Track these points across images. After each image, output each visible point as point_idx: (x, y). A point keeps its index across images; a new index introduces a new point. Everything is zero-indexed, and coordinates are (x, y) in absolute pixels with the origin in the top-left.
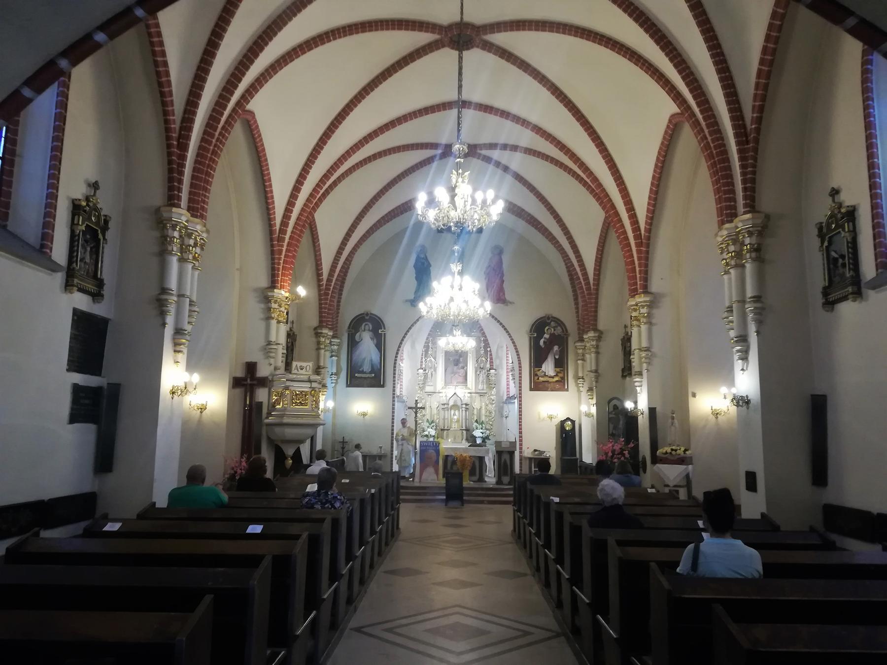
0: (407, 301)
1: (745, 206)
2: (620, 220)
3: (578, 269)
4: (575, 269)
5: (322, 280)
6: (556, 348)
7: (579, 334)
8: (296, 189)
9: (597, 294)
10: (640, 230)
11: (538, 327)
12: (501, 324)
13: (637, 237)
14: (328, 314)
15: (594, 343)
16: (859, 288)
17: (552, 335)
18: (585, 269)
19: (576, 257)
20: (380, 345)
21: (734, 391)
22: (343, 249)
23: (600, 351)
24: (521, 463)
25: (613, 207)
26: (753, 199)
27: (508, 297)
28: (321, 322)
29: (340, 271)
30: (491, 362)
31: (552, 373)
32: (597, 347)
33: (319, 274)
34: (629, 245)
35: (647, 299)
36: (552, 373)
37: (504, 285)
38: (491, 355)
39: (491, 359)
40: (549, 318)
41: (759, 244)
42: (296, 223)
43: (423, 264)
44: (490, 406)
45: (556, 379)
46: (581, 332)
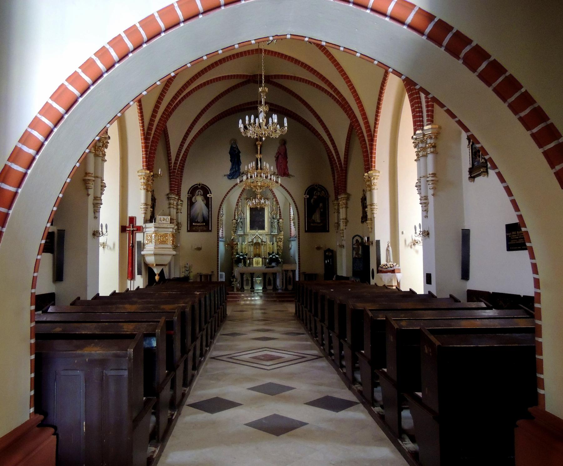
1: (428, 121)
2: (359, 125)
4: (332, 154)
5: (171, 163)
6: (321, 205)
7: (335, 195)
8: (182, 145)
11: (311, 191)
13: (341, 167)
14: (176, 185)
15: (344, 201)
16: (487, 170)
18: (338, 154)
19: (333, 147)
20: (208, 202)
22: (184, 143)
24: (299, 276)
25: (355, 116)
26: (432, 117)
27: (290, 172)
28: (171, 190)
30: (280, 215)
31: (319, 221)
32: (347, 204)
33: (169, 160)
34: (364, 140)
36: (319, 221)
37: (288, 165)
38: (280, 210)
39: (280, 212)
40: (316, 185)
41: (435, 144)
42: (156, 128)
43: (235, 151)
46: (337, 194)
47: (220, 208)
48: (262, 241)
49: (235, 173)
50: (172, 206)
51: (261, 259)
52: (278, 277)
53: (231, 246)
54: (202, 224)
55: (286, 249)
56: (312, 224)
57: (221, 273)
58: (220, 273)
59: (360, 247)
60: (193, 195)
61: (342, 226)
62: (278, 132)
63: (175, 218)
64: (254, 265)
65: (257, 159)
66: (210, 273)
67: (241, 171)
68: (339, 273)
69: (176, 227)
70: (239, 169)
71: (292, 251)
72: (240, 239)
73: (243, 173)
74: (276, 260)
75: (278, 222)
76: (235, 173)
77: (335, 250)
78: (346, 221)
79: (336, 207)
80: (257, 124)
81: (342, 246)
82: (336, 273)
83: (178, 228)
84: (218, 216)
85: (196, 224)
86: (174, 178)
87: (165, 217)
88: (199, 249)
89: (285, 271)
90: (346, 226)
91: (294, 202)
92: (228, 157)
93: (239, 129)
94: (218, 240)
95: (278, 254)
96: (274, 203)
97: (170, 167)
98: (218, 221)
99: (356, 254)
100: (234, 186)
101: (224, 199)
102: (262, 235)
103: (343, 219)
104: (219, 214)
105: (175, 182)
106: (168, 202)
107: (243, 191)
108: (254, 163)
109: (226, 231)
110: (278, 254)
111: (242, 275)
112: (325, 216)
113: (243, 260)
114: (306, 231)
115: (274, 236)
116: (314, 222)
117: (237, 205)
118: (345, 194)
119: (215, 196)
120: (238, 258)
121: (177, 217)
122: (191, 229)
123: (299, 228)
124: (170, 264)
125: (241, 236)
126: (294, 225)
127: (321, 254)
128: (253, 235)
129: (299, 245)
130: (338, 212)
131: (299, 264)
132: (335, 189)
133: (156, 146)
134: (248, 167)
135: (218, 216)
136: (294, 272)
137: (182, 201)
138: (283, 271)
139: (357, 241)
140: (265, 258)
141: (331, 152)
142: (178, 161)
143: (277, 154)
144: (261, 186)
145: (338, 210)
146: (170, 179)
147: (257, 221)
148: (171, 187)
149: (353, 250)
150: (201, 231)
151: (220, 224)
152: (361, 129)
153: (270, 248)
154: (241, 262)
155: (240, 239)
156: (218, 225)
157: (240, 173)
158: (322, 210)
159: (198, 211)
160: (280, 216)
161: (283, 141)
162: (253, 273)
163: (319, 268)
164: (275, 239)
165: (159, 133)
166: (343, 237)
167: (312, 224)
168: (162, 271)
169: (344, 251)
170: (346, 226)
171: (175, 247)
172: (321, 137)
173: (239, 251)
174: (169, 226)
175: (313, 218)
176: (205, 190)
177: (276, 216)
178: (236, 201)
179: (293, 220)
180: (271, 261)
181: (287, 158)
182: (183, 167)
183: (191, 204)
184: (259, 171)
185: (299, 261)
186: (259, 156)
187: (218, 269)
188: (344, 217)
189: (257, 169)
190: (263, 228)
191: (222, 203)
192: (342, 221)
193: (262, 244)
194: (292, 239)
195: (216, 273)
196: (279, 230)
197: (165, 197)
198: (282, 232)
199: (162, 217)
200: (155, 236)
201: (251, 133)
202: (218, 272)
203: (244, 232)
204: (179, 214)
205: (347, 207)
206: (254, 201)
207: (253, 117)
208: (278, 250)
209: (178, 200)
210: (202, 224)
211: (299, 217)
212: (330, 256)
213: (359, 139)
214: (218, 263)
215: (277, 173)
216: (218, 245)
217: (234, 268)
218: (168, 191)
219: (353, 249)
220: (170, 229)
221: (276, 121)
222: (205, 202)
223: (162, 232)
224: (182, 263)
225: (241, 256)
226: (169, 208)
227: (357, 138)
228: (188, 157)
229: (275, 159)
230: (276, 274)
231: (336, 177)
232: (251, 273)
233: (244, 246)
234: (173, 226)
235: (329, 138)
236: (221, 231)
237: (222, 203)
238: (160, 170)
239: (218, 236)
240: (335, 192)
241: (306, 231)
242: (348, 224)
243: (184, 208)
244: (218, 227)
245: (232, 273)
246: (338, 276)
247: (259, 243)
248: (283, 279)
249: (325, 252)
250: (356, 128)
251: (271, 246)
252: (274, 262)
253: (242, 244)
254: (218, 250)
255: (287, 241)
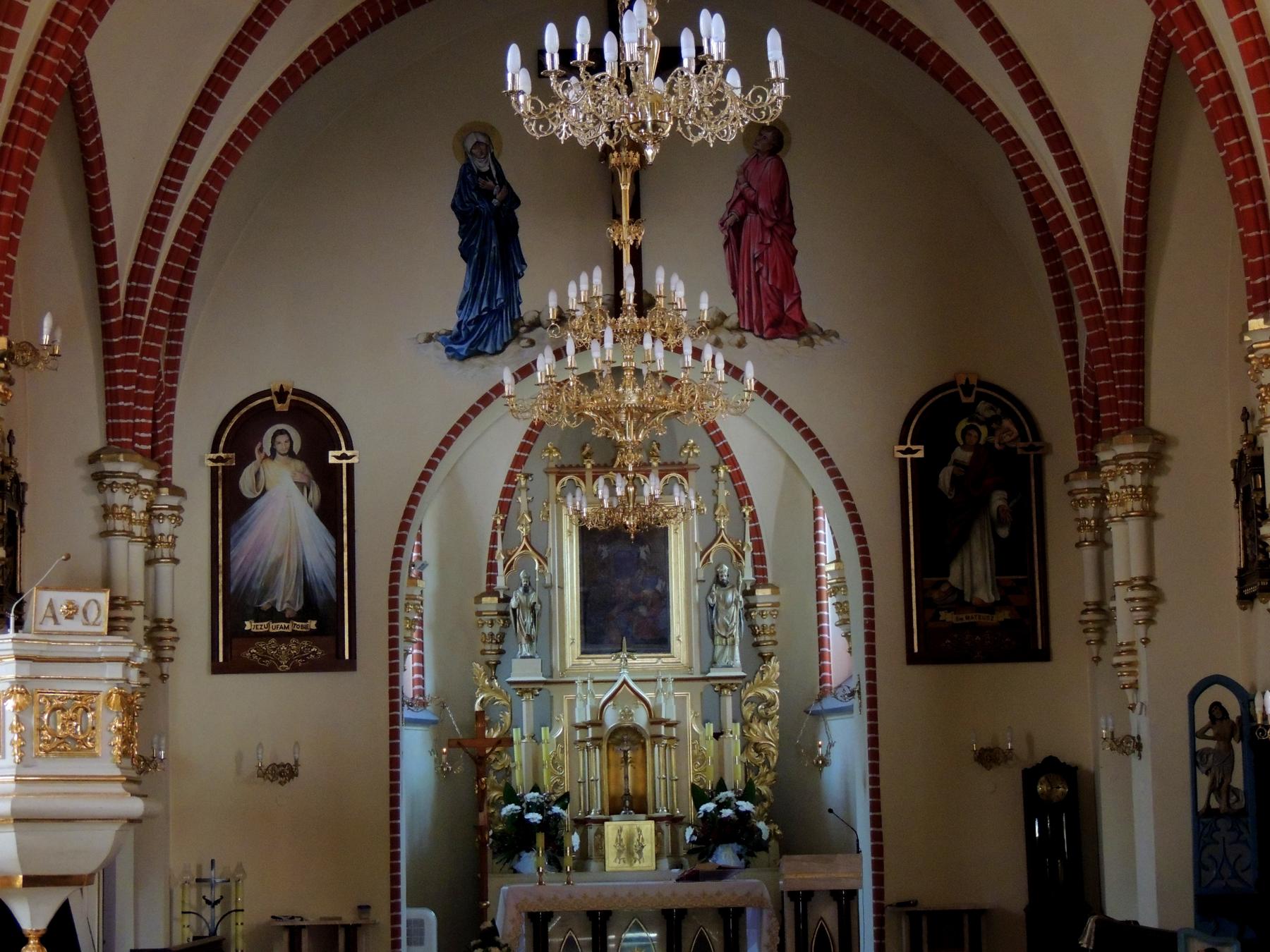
0: (430, 338)
2: (1207, 39)
3: (1068, 207)
4: (1057, 206)
5: (114, 273)
6: (998, 500)
7: (1082, 443)
8: (175, 170)
9: (1140, 297)
10: (1113, 263)
11: (935, 420)
12: (790, 415)
13: (1110, 278)
14: (139, 399)
15: (1136, 479)
17: (983, 452)
19: (1061, 162)
20: (332, 498)
21: (33, 942)
22: (189, 156)
23: (1159, 507)
24: (879, 922)
27: (814, 310)
28: (111, 431)
29: (179, 237)
30: (759, 560)
31: (985, 595)
32: (1149, 493)
33: (103, 255)
35: (1144, 448)
36: (985, 595)
37: (799, 269)
38: (756, 531)
39: (758, 546)
40: (967, 389)
42: (26, 80)
43: (488, 195)
44: (757, 727)
45: (1003, 615)
46: (1091, 434)
47: (404, 526)
48: (655, 721)
49: (492, 320)
50: (120, 525)
51: (647, 827)
52: (751, 933)
53: (473, 751)
54: (298, 626)
55: (801, 757)
56: (947, 617)
57: (418, 913)
58: (405, 913)
59: (1238, 748)
60: (245, 457)
61: (1125, 626)
62: (732, 109)
63: (138, 595)
64: (613, 862)
65: (618, 254)
66: (349, 918)
67: (527, 310)
68: (1116, 909)
69: (145, 654)
70: (512, 299)
71: (832, 777)
72: (527, 708)
73: (536, 324)
74: (738, 831)
75: (749, 607)
76: (492, 320)
77: (1086, 763)
78: (1151, 595)
79: (1089, 511)
80: (611, 69)
81: (1129, 745)
82: (1098, 906)
83: (159, 659)
84: (394, 577)
85: (261, 627)
86: (128, 362)
87: (81, 598)
88: (283, 773)
89: (793, 895)
90: (1149, 621)
91: (840, 484)
92: (449, 231)
93: (505, 99)
94: (394, 720)
95: (748, 793)
96: (725, 492)
97: (105, 296)
98: (393, 604)
99: (1213, 789)
100: (486, 400)
101: (425, 476)
102: (654, 682)
103: (1129, 584)
104: (396, 565)
105: (140, 383)
106: (94, 501)
107: (530, 436)
108: (598, 274)
109: (440, 663)
110: (748, 793)
111: (539, 922)
112: (1022, 561)
113: (539, 832)
114: (912, 659)
115: (723, 685)
116: (958, 600)
117: (504, 507)
118: (1138, 439)
119: (377, 462)
120: (518, 820)
121: (152, 585)
122: (236, 653)
123: (870, 637)
124: (108, 872)
125: (525, 688)
126: (843, 622)
127: (1003, 787)
128: (602, 683)
129: (873, 742)
130: (1102, 543)
131: (877, 851)
132: (1078, 407)
133: (27, 180)
134: (563, 296)
135: (394, 577)
136: (845, 900)
137: (177, 491)
138: (779, 898)
139: (1217, 710)
140: (674, 821)
141: (1049, 191)
142: (152, 258)
143: (732, 206)
144: (642, 409)
145: (1101, 526)
146: (109, 365)
147: (623, 604)
148: (111, 413)
149: (1195, 764)
150: (295, 669)
151: (402, 624)
152: (1216, 60)
153: (700, 758)
154: (529, 846)
155: (527, 708)
156: (393, 630)
157: (516, 321)
158: (1004, 532)
159: (274, 551)
160: (760, 572)
161: (768, 141)
162: (607, 914)
163: (996, 876)
164: (728, 702)
165: (46, 107)
166: (1134, 686)
167: (947, 617)
168: (64, 914)
169: (1141, 770)
170: (1149, 621)
171: (142, 768)
172: (990, 105)
173: (520, 779)
174: (101, 651)
175: (954, 579)
176: (317, 427)
177: (739, 570)
178: (500, 483)
179: (835, 591)
180: (713, 833)
181: (791, 231)
182: (184, 292)
183: (232, 507)
184: (629, 319)
185: (876, 836)
186: (625, 234)
187: (395, 894)
188: (1137, 571)
189: (615, 306)
190: (656, 638)
191: (414, 500)
192: (1121, 593)
193: (656, 737)
194: (829, 703)
195: (381, 914)
196: (757, 654)
197: (79, 475)
198: (774, 664)
199: (61, 599)
200: (19, 708)
201: (579, 115)
202: (395, 907)
203: (548, 668)
204: (165, 569)
205: (1149, 515)
206: (603, 492)
207: (583, 30)
208: (747, 767)
209: (157, 485)
210: (298, 626)
211: (867, 575)
212: (1060, 807)
213: (1212, 118)
214: (395, 856)
215: (733, 320)
216: (395, 749)
217: (492, 882)
218: (96, 439)
219: (1197, 759)
220: (109, 667)
221: (717, 47)
222: (315, 494)
223: (63, 682)
224: (182, 857)
225: (532, 807)
226: (107, 534)
227: (1199, 114)
228: (210, 233)
229: (721, 238)
230: (740, 912)
231: (1083, 335)
232: (592, 915)
233: (547, 752)
234: (123, 646)
235: (1035, 111)
236: (410, 664)
237: (414, 500)
238: (47, 323)
239: (394, 694)
240: (1081, 426)
241: (912, 659)
242: (1162, 610)
243: (193, 533)
244: (393, 643)
245: (481, 914)
246: (1108, 927)
247: (635, 730)
248: (782, 934)
249: (1030, 776)
250: (1189, 55)
251: (710, 746)
252: (726, 840)
253: (536, 737)
254: (395, 776)
255: (804, 714)
